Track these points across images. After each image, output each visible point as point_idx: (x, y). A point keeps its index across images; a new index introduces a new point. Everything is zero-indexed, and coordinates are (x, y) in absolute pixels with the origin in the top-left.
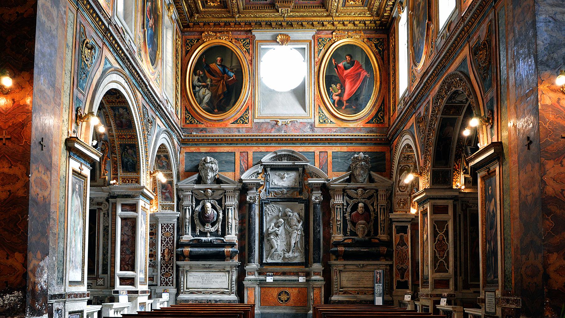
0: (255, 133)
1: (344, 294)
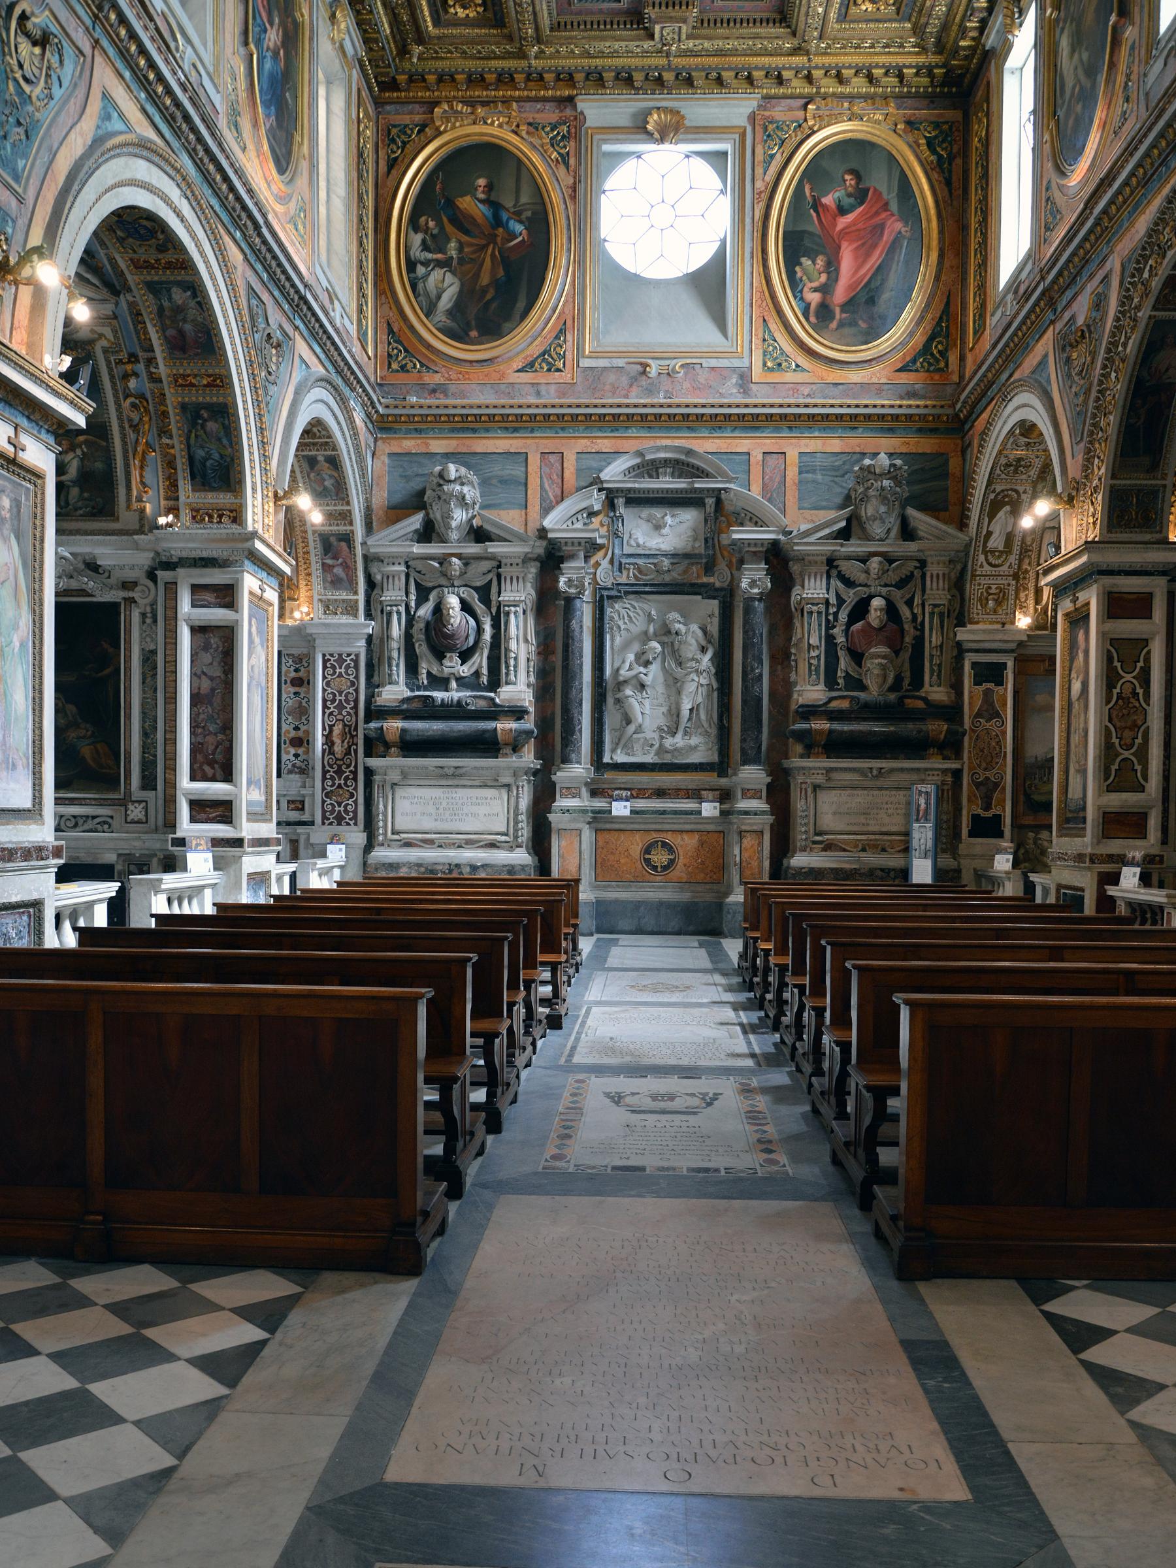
0: (582, 399)
1: (824, 850)
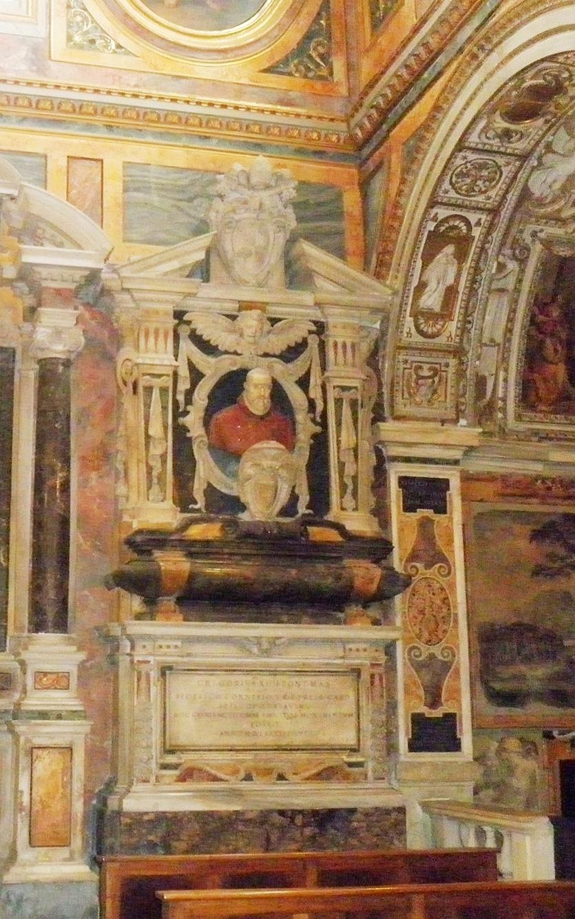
1: (182, 779)
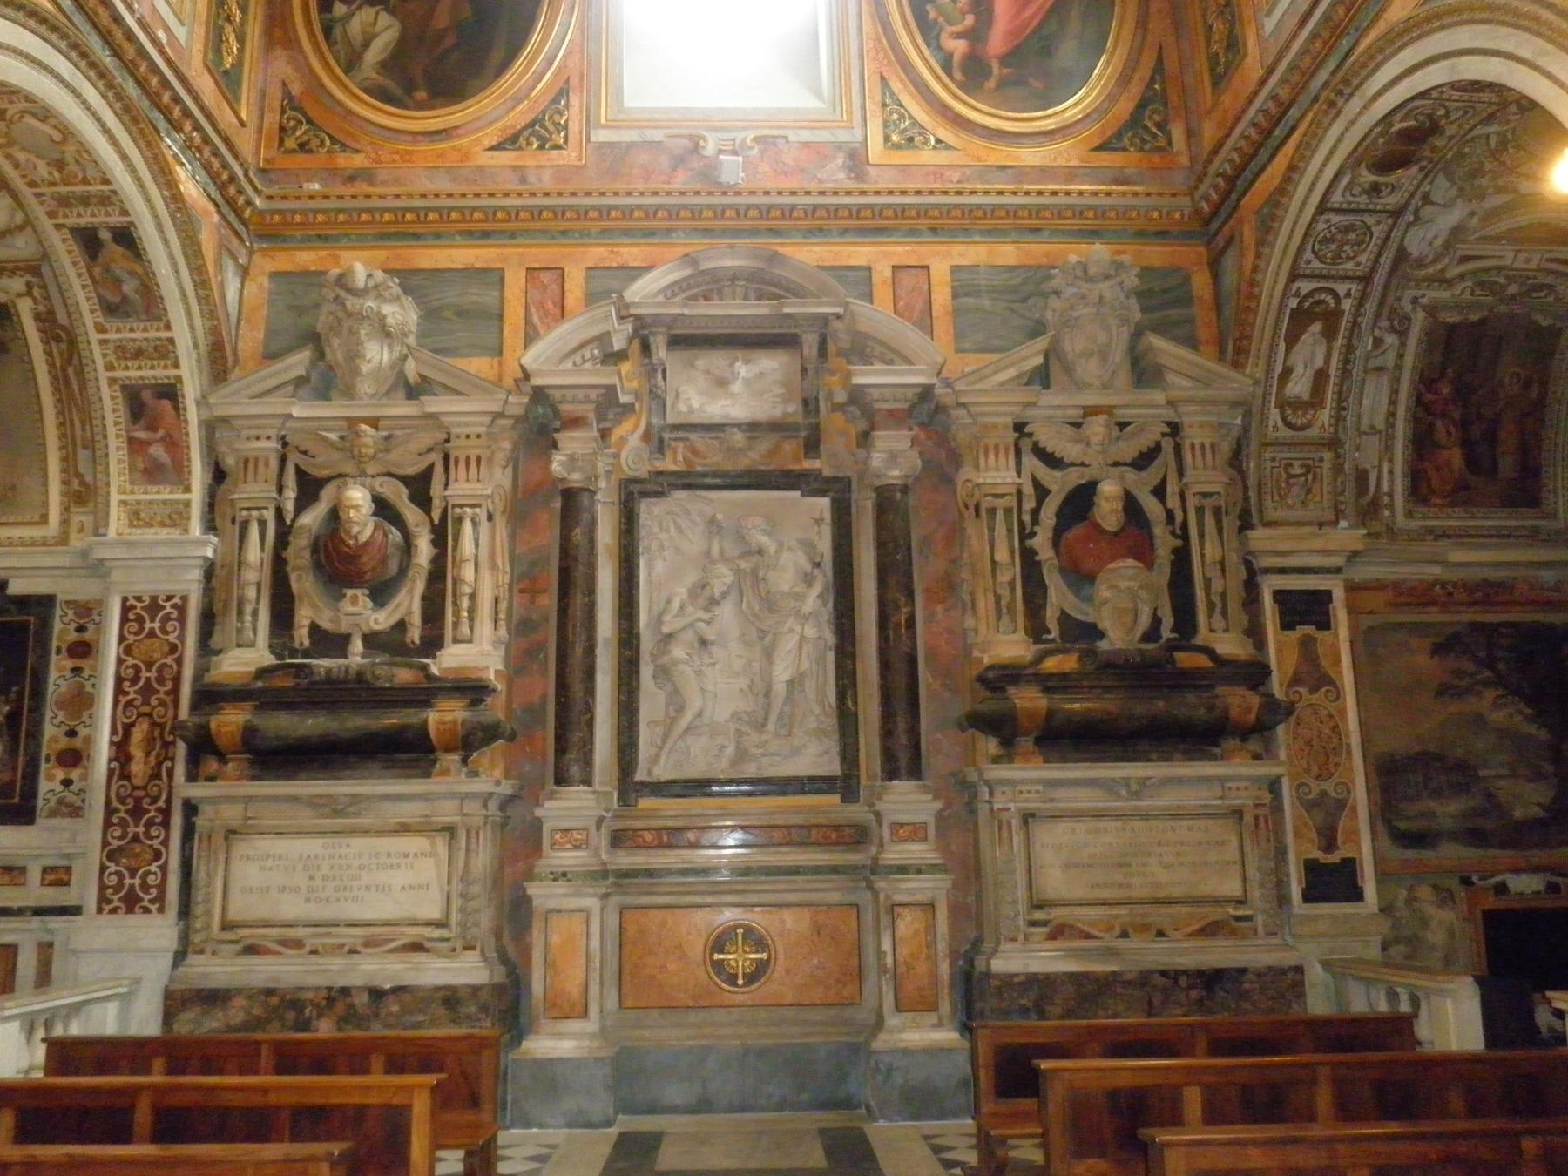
1: (1052, 937)
